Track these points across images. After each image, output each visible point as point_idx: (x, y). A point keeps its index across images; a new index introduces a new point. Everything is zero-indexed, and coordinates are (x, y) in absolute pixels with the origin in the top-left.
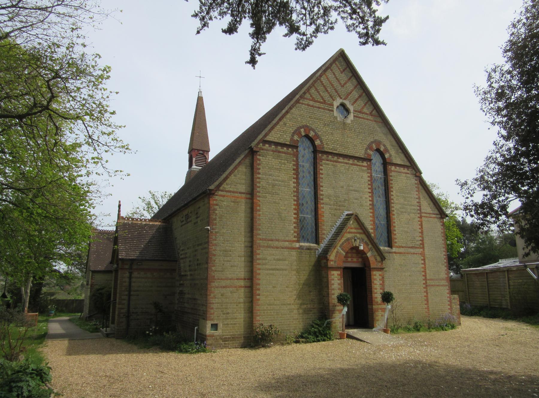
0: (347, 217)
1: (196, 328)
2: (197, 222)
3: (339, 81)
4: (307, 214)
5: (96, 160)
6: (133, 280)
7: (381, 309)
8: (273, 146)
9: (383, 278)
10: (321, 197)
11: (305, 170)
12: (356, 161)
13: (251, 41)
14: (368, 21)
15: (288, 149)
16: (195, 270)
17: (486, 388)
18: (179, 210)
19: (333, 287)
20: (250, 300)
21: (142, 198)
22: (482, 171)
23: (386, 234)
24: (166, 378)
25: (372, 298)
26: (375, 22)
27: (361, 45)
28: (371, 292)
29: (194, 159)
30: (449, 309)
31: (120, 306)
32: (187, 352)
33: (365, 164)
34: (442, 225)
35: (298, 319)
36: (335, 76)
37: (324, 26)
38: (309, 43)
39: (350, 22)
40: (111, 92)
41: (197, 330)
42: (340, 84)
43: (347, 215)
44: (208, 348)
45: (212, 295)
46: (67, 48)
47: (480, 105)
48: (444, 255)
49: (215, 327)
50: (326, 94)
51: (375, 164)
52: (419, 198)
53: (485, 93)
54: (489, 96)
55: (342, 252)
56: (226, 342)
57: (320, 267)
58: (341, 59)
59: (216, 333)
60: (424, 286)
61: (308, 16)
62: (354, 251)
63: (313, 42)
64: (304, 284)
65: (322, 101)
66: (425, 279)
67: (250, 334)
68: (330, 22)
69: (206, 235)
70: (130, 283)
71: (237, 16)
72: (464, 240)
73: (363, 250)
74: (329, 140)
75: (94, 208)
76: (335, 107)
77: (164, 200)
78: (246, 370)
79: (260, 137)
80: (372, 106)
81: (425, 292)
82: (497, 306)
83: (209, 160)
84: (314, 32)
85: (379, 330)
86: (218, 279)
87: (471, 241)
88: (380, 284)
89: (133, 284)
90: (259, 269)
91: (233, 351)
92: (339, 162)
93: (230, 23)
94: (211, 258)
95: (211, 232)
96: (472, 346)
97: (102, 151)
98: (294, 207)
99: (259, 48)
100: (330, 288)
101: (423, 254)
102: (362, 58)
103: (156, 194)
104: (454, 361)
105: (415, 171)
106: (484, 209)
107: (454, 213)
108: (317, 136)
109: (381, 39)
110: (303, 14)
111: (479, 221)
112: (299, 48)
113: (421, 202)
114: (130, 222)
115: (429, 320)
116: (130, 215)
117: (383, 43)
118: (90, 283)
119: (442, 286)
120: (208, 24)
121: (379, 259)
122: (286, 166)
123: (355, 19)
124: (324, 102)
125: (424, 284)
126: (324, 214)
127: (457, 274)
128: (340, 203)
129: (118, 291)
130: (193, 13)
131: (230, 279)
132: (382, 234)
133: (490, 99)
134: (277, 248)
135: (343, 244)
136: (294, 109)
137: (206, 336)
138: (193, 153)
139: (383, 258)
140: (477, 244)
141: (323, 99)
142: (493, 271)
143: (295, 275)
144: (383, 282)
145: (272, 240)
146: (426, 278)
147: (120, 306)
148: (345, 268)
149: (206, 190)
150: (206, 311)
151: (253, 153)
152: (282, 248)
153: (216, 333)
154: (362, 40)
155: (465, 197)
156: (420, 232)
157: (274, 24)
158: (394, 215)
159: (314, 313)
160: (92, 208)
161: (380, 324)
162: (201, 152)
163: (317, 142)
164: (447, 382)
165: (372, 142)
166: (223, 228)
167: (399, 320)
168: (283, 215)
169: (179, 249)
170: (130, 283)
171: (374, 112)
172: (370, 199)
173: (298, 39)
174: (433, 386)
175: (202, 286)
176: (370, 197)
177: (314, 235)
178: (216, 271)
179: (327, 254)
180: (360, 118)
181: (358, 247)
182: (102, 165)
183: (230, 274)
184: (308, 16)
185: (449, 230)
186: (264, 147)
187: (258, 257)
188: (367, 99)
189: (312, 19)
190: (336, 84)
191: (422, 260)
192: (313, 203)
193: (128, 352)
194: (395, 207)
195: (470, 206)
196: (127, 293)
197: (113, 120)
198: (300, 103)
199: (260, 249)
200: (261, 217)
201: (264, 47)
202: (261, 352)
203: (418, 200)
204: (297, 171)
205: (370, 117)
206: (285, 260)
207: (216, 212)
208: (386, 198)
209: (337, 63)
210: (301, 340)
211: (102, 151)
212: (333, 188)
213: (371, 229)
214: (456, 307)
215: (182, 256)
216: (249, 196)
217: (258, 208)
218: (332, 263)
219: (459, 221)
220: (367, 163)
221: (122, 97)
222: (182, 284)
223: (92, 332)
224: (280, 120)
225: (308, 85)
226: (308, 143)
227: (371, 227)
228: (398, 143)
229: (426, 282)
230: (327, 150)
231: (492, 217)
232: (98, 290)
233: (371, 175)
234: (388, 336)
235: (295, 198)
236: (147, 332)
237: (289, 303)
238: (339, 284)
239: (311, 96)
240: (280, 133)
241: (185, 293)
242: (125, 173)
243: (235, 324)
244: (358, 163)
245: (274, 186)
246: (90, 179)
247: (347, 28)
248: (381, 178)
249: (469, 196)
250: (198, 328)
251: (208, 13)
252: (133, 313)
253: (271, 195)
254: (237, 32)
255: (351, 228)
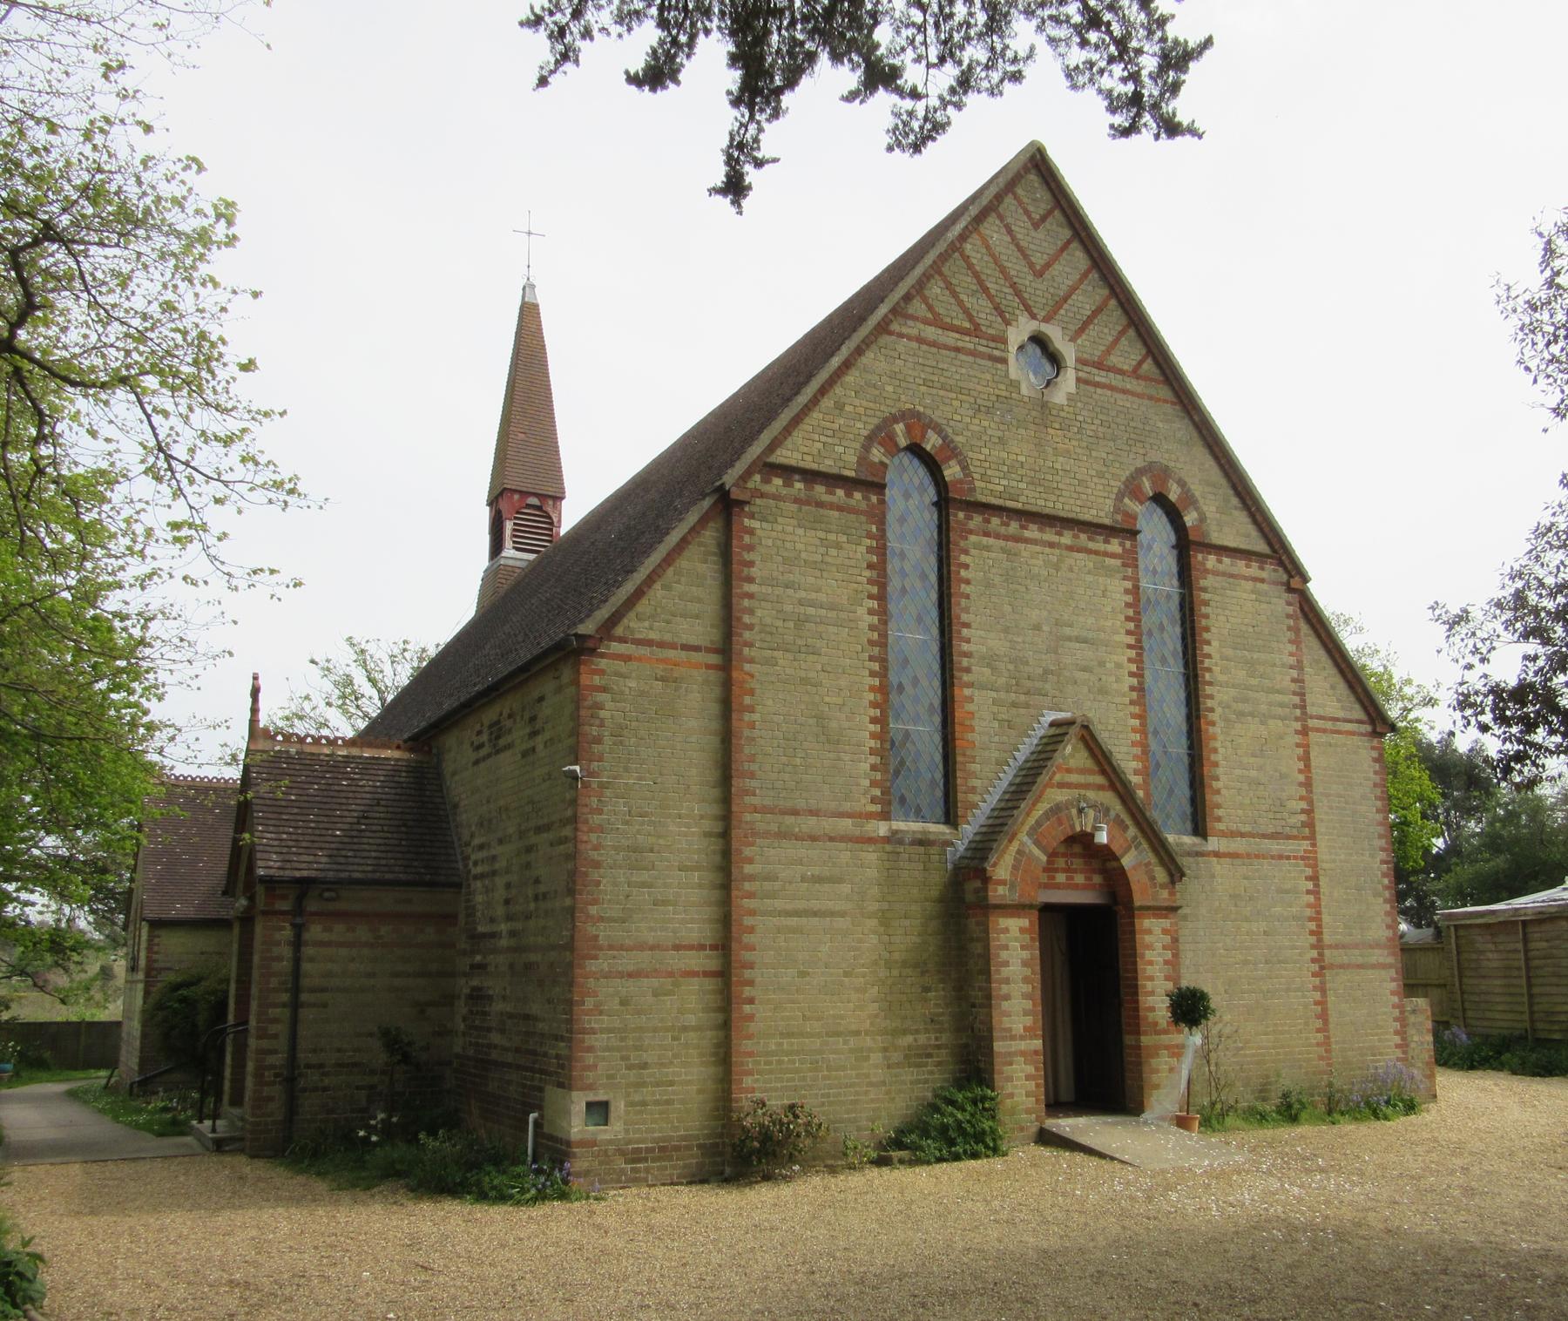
0: (1053, 731)
1: (532, 1117)
2: (533, 749)
3: (1025, 256)
4: (916, 720)
5: (185, 532)
6: (308, 951)
7: (1167, 1048)
8: (799, 485)
9: (1175, 940)
10: (965, 662)
11: (907, 567)
12: (1083, 537)
13: (728, 118)
14: (1139, 52)
15: (849, 495)
16: (528, 917)
17: (1529, 1307)
18: (468, 708)
19: (1005, 972)
20: (720, 1017)
21: (323, 664)
22: (1520, 575)
23: (1187, 792)
24: (444, 1287)
25: (1137, 1009)
26: (1165, 56)
27: (1114, 137)
28: (1134, 989)
29: (509, 526)
30: (1397, 1046)
31: (265, 1044)
32: (502, 1198)
33: (1115, 546)
34: (1375, 760)
35: (884, 1083)
36: (1013, 238)
37: (987, 67)
38: (935, 127)
39: (1077, 56)
40: (234, 292)
41: (537, 1124)
42: (1031, 265)
43: (1052, 724)
44: (576, 1184)
45: (589, 1003)
46: (88, 136)
47: (1517, 347)
48: (1383, 862)
49: (599, 1111)
50: (984, 302)
51: (1150, 548)
52: (1299, 666)
53: (1534, 308)
54: (1546, 316)
55: (1036, 851)
56: (639, 1164)
57: (962, 902)
58: (1033, 177)
59: (604, 1133)
60: (1315, 967)
61: (931, 31)
62: (1077, 849)
63: (949, 123)
64: (904, 964)
65: (967, 325)
66: (1319, 946)
67: (721, 1136)
68: (1010, 54)
69: (568, 796)
70: (297, 961)
71: (680, 26)
72: (1447, 811)
73: (1106, 847)
74: (995, 463)
75: (160, 698)
76: (1013, 348)
77: (399, 668)
78: (716, 1259)
79: (755, 450)
80: (1139, 345)
81: (1315, 988)
82: (1557, 1036)
83: (563, 531)
84: (952, 91)
85: (1163, 1119)
86: (611, 947)
87: (1469, 812)
88: (1166, 962)
89: (306, 967)
90: (752, 913)
91: (663, 1194)
92: (1027, 541)
93: (654, 51)
94: (586, 874)
95: (586, 786)
96: (1476, 1170)
97: (205, 499)
98: (871, 696)
99: (756, 140)
100: (995, 977)
101: (1311, 859)
102: (1119, 187)
103: (371, 648)
104: (1418, 1221)
105: (1285, 569)
106: (1524, 704)
107: (1411, 716)
108: (950, 449)
109: (1183, 118)
110: (914, 24)
111: (1508, 746)
112: (899, 144)
113: (1307, 678)
114: (293, 750)
115: (1330, 1085)
116: (280, 724)
117: (1193, 131)
118: (142, 962)
119: (1373, 966)
120: (576, 51)
121: (1161, 875)
122: (843, 553)
123: (1097, 47)
124: (975, 331)
125: (1313, 961)
126: (976, 723)
127: (1418, 926)
128: (1028, 684)
129: (254, 991)
130: (526, 14)
131: (652, 948)
132: (1171, 792)
133: (1551, 329)
134: (813, 838)
135: (1038, 823)
136: (870, 355)
137: (568, 1143)
138: (504, 505)
139: (1176, 874)
140: (1491, 824)
141: (971, 318)
142: (1545, 918)
143: (875, 932)
144: (1176, 955)
145: (795, 812)
146: (1320, 940)
147: (265, 1044)
148: (1047, 910)
149: (566, 639)
150: (570, 1058)
151: (727, 506)
152: (832, 839)
153: (604, 1133)
154: (1120, 120)
155: (1462, 662)
156: (1301, 784)
157: (811, 57)
158: (1213, 724)
159: (939, 1064)
160: (154, 700)
161: (1164, 1097)
162: (534, 501)
163: (951, 471)
164: (1398, 1290)
165: (1140, 472)
166: (626, 770)
167: (1230, 1085)
168: (834, 724)
169: (467, 844)
170: (297, 961)
171: (1148, 366)
172: (1133, 668)
173: (897, 115)
174: (1353, 1301)
175: (555, 970)
176: (1130, 660)
177: (939, 793)
178: (601, 919)
179: (985, 859)
180: (1097, 385)
181: (1093, 836)
182: (206, 548)
183: (651, 929)
184: (931, 31)
185: (1395, 774)
186: (766, 488)
187: (748, 869)
188: (1124, 321)
189: (945, 43)
190: (1016, 266)
191: (1308, 878)
192: (937, 683)
193: (295, 1200)
194: (1218, 697)
195: (1476, 693)
196: (285, 997)
197: (246, 390)
198: (891, 333)
199: (752, 845)
200: (756, 733)
201: (773, 137)
202: (760, 1201)
203: (1294, 673)
204: (879, 570)
205: (1131, 384)
206: (840, 881)
207: (602, 714)
208: (1186, 665)
209: (1019, 191)
210: (896, 1154)
211: (205, 499)
212: (1006, 630)
213: (1136, 772)
214: (1422, 1041)
215: (479, 870)
216: (714, 659)
217: (747, 700)
218: (1001, 890)
219: (1430, 745)
220: (1121, 544)
221: (258, 308)
222: (481, 967)
223: (160, 1135)
224: (823, 391)
225: (918, 271)
226: (916, 473)
227: (1134, 764)
228: (1227, 475)
229: (1321, 955)
230: (983, 499)
231: (1552, 732)
232: (177, 987)
233: (1136, 587)
234: (1193, 1138)
235: (876, 666)
236: (362, 1133)
237: (854, 1027)
238: (1025, 964)
239: (930, 308)
240: (824, 438)
241: (490, 998)
242: (284, 577)
243: (668, 1102)
244: (1091, 545)
245: (801, 622)
246: (154, 597)
247: (1069, 76)
248: (1169, 596)
249: (1475, 660)
250: (542, 1116)
251: (577, 14)
252: (308, 1066)
253: (789, 656)
254: (677, 83)
255: (1069, 771)
